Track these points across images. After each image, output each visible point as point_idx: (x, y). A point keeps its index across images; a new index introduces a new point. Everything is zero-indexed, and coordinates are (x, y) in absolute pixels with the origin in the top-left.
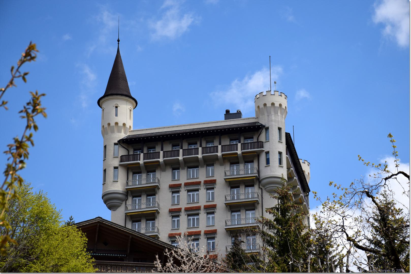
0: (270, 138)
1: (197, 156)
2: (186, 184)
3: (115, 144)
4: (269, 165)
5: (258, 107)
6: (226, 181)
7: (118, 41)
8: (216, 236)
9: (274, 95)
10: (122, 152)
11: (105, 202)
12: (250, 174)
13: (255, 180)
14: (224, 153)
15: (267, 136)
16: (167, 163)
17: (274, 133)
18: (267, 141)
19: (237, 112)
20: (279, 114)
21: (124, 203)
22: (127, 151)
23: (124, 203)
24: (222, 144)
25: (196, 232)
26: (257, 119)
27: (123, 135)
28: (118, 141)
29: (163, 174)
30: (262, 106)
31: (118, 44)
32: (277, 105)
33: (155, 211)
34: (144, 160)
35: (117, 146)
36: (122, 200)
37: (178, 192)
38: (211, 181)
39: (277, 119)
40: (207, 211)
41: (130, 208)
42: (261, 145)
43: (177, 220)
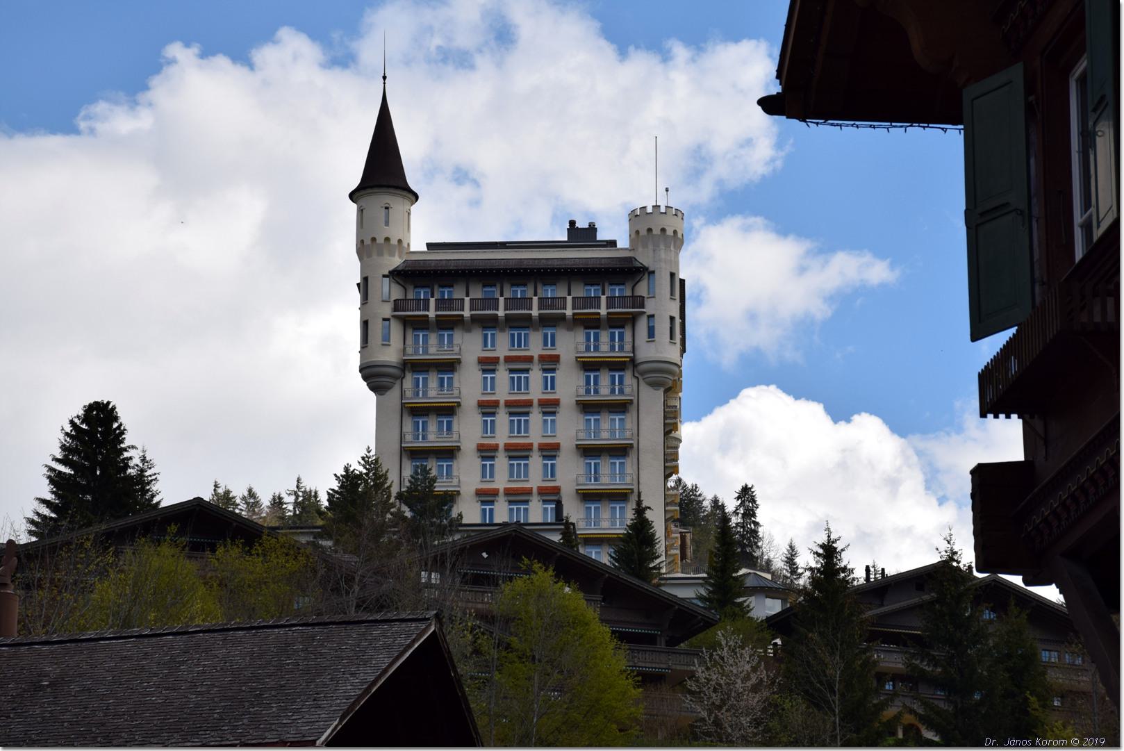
0: (657, 291)
1: (530, 312)
2: (508, 359)
3: (384, 276)
4: (653, 339)
5: (637, 232)
6: (576, 360)
7: (384, 78)
8: (558, 453)
9: (665, 213)
10: (397, 293)
11: (365, 378)
14: (576, 311)
15: (651, 286)
16: (474, 319)
18: (650, 296)
19: (590, 226)
20: (672, 248)
21: (398, 382)
22: (402, 288)
23: (398, 382)
25: (524, 445)
26: (632, 252)
27: (396, 262)
28: (390, 272)
29: (467, 336)
30: (643, 232)
31: (384, 83)
32: (670, 232)
33: (456, 404)
35: (388, 279)
36: (395, 377)
37: (493, 371)
38: (550, 356)
39: (669, 258)
40: (544, 410)
41: (409, 394)
42: (639, 302)
43: (491, 420)
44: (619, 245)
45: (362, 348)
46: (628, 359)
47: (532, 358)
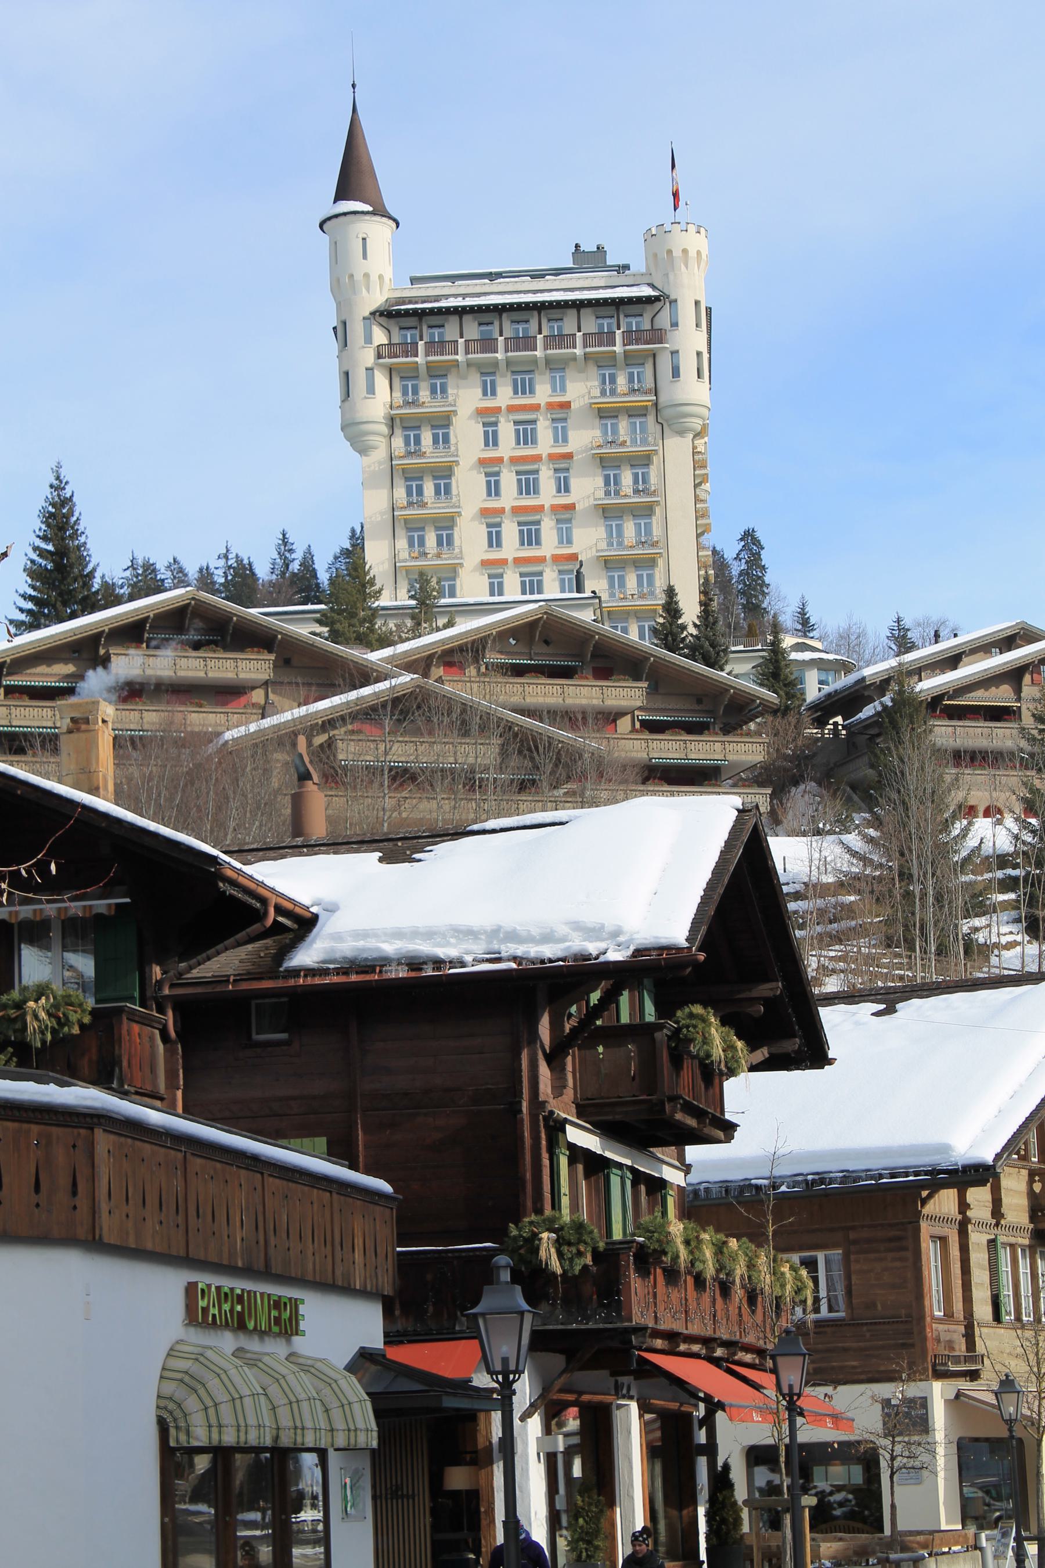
7: (354, 86)
10: (380, 337)
12: (656, 395)
13: (649, 408)
16: (548, 361)
17: (687, 314)
19: (598, 248)
24: (584, 330)
34: (624, 345)
44: (633, 269)
45: (341, 351)
46: (650, 403)
47: (539, 405)
